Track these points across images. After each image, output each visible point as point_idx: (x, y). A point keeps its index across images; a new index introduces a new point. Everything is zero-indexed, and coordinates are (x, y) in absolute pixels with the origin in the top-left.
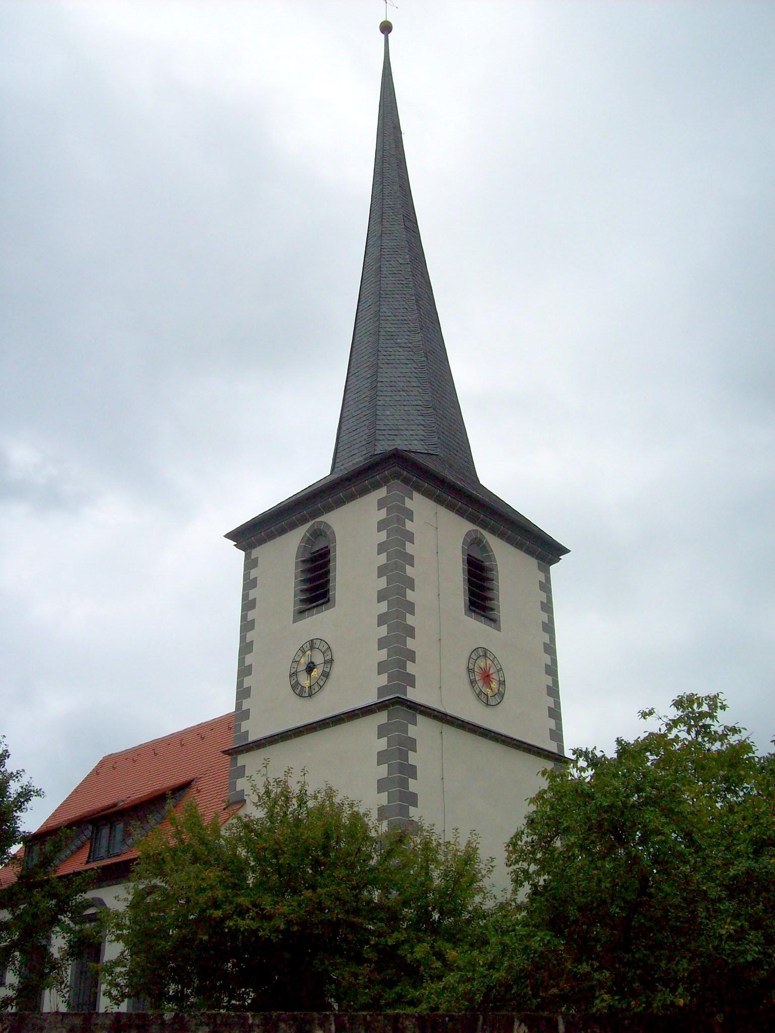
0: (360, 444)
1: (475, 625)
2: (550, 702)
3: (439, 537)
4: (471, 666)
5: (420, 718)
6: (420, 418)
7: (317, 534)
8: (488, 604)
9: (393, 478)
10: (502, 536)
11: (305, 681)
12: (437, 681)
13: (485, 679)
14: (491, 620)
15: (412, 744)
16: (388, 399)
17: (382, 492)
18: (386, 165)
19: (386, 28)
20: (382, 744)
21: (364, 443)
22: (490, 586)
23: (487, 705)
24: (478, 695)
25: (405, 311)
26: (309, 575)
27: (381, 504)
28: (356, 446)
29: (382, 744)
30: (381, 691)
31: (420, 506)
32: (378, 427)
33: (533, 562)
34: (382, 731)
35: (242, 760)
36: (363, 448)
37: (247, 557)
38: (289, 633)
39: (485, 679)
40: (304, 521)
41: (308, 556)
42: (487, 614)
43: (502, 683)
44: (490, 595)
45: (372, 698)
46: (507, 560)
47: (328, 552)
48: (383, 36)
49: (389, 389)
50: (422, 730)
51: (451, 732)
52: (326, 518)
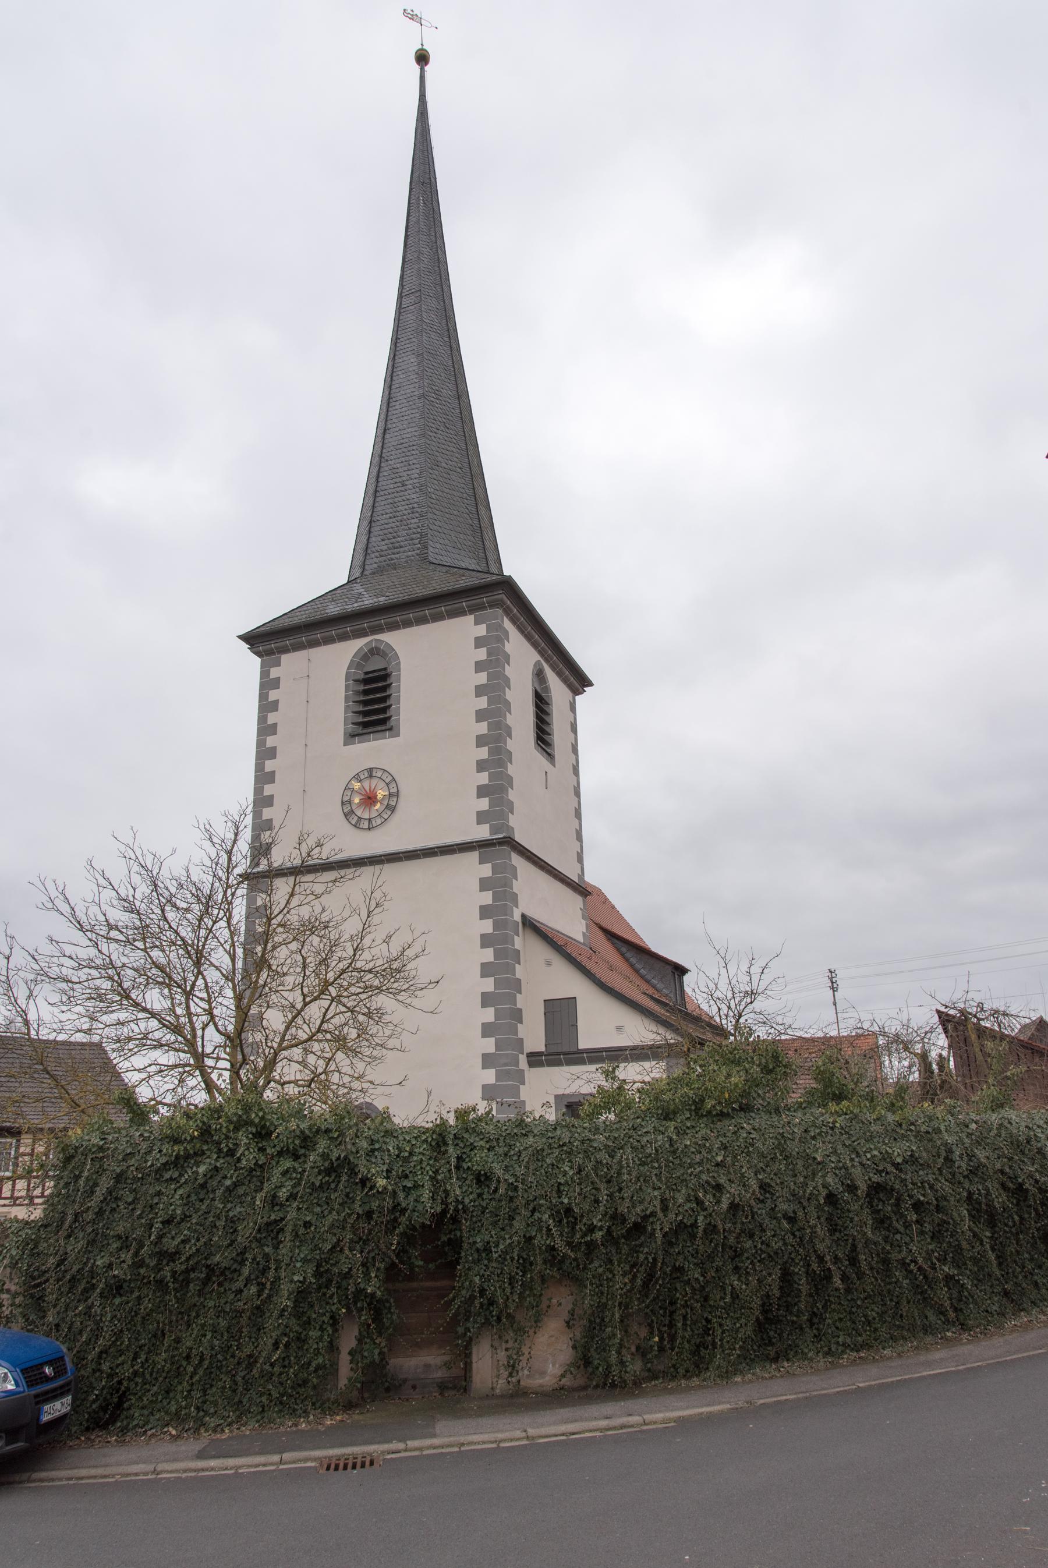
14: (549, 754)
19: (422, 58)
26: (361, 719)
48: (417, 68)
52: (391, 638)
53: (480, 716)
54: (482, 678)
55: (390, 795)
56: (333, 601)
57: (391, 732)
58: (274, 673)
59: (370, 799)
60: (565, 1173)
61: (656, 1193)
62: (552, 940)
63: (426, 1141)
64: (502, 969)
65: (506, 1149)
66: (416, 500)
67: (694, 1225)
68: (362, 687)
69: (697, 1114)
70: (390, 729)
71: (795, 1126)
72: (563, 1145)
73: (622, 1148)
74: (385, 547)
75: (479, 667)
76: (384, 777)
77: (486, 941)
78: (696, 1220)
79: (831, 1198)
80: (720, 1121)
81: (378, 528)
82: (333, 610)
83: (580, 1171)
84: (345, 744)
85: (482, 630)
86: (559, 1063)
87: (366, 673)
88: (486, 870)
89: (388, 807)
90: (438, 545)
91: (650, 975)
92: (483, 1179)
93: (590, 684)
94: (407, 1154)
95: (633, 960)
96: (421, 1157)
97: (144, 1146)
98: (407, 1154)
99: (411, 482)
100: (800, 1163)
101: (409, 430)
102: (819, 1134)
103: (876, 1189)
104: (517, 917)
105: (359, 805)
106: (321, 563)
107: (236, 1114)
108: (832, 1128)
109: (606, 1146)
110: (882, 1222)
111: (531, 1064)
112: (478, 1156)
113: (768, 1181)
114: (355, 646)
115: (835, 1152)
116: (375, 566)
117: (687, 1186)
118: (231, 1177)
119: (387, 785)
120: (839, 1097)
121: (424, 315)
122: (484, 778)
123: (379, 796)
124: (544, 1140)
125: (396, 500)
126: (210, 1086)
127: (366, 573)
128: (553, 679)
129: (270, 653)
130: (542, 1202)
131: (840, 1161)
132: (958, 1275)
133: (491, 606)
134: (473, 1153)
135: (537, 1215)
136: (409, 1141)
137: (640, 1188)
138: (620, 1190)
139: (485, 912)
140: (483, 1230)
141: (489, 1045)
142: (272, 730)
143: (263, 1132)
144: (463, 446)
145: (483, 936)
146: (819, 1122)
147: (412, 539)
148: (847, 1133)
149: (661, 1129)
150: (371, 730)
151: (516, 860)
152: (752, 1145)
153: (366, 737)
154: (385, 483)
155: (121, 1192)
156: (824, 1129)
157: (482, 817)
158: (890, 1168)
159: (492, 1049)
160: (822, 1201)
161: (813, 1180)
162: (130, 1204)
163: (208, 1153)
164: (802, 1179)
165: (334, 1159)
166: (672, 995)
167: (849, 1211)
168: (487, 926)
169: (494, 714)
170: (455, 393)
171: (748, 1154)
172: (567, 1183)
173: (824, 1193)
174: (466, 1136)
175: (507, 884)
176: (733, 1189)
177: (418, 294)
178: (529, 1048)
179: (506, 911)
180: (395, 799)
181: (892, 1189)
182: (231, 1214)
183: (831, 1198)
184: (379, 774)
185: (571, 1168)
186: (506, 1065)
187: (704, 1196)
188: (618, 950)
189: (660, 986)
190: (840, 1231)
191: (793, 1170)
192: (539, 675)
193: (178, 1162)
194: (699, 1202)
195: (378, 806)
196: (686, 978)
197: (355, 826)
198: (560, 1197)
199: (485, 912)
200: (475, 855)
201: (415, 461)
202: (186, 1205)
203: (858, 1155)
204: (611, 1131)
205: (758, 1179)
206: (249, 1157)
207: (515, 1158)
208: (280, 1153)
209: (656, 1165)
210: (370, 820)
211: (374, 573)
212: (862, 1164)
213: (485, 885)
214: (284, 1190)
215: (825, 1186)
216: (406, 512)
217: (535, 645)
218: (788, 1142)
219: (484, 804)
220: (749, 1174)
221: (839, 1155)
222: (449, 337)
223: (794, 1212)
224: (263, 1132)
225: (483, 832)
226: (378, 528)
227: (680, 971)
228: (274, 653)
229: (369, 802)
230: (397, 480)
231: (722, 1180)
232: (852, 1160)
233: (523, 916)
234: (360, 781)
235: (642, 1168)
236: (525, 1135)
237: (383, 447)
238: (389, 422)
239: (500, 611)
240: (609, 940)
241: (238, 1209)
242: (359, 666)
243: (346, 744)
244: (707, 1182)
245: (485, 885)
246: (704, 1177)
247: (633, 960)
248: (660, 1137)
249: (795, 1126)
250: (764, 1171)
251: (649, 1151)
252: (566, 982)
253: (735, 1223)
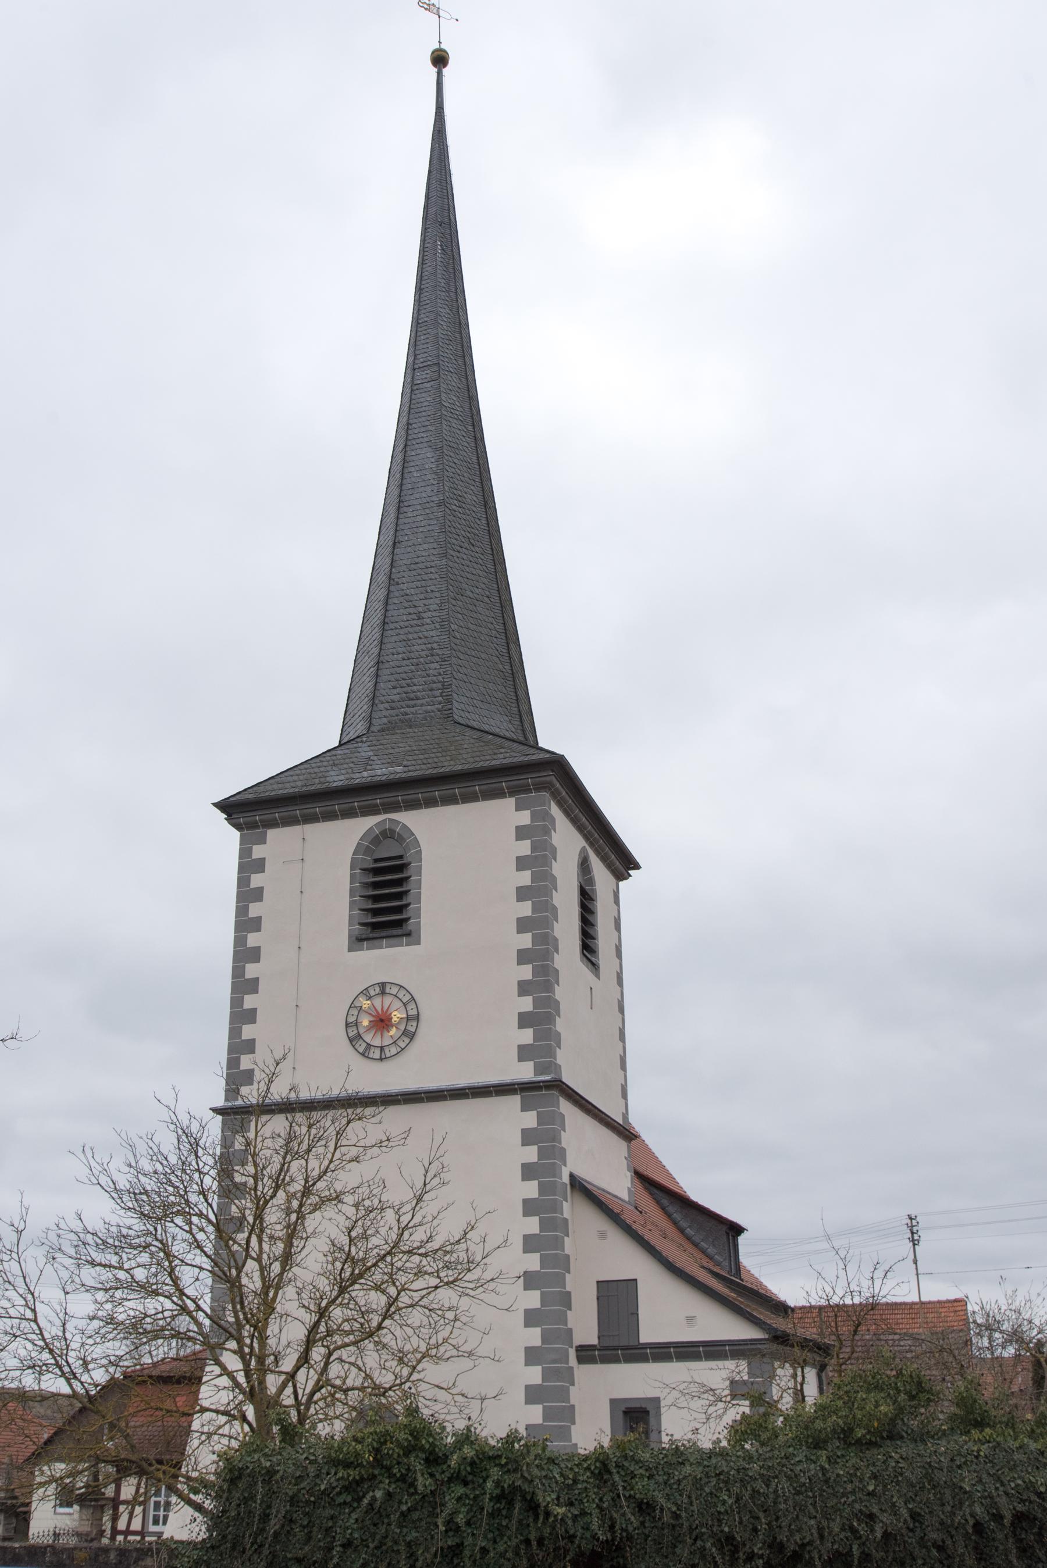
14: (593, 964)
19: (440, 59)
48: (435, 70)
53: (523, 925)
54: (525, 878)
55: (409, 1018)
56: (334, 765)
57: (410, 939)
58: (258, 852)
59: (382, 1022)
60: (724, 1502)
61: (812, 1522)
62: (607, 1207)
63: (588, 1468)
64: (548, 1242)
65: (665, 1478)
66: (436, 639)
67: (849, 1553)
69: (845, 1442)
70: (408, 934)
71: (941, 1455)
72: (720, 1474)
73: (776, 1477)
74: (397, 697)
75: (522, 863)
76: (400, 995)
77: (529, 1207)
78: (851, 1548)
79: (978, 1527)
80: (868, 1449)
81: (388, 672)
82: (337, 779)
83: (737, 1500)
84: (349, 950)
85: (524, 818)
86: (616, 1360)
87: (376, 861)
88: (530, 1120)
89: (405, 1033)
90: (463, 699)
91: (701, 1239)
92: (645, 1507)
93: (637, 867)
94: (571, 1482)
95: (677, 1216)
96: (585, 1485)
97: (312, 1470)
98: (571, 1482)
99: (429, 614)
100: (948, 1493)
101: (426, 546)
102: (965, 1463)
103: (1019, 1517)
104: (566, 1179)
105: (368, 1029)
106: (306, 719)
107: (407, 1439)
108: (977, 1457)
109: (762, 1475)
110: (1024, 1551)
111: (581, 1360)
112: (639, 1485)
113: (918, 1510)
114: (361, 826)
115: (980, 1481)
116: (385, 720)
117: (841, 1516)
118: (406, 1503)
119: (405, 1005)
120: (980, 1424)
121: (444, 396)
122: (526, 1004)
123: (395, 1019)
124: (701, 1468)
125: (410, 636)
127: (373, 729)
128: (597, 865)
129: (253, 826)
130: (704, 1530)
131: (985, 1491)
133: (537, 790)
134: (634, 1481)
135: (699, 1543)
136: (571, 1469)
137: (797, 1516)
138: (777, 1519)
139: (528, 1172)
140: (647, 1558)
141: (534, 1337)
142: (255, 925)
143: (431, 1458)
144: (491, 568)
145: (525, 1202)
146: (964, 1451)
147: (431, 690)
148: (991, 1462)
149: (812, 1457)
150: (382, 934)
151: (565, 1107)
152: (901, 1474)
153: (376, 942)
154: (395, 613)
155: (295, 1515)
156: (969, 1458)
157: (524, 1053)
158: (1034, 1498)
159: (537, 1342)
160: (970, 1531)
161: (961, 1509)
162: (304, 1527)
163: (380, 1478)
164: (949, 1509)
165: (506, 1486)
166: (726, 1264)
167: (993, 1539)
168: (531, 1189)
169: (538, 923)
170: (481, 498)
171: (898, 1483)
172: (726, 1511)
173: (971, 1522)
174: (626, 1464)
175: (555, 1138)
176: (885, 1518)
177: (435, 368)
178: (579, 1339)
179: (553, 1171)
180: (415, 1024)
181: (1035, 1519)
182: (408, 1539)
183: (978, 1527)
184: (394, 990)
185: (730, 1497)
186: (554, 1361)
187: (859, 1525)
188: (658, 1202)
189: (711, 1250)
190: (985, 1560)
191: (941, 1499)
192: (584, 866)
193: (353, 1487)
194: (853, 1530)
195: (393, 1031)
196: (742, 1239)
197: (363, 1054)
198: (720, 1526)
199: (528, 1172)
200: (515, 1100)
201: (433, 588)
202: (361, 1529)
203: (1003, 1484)
204: (765, 1460)
205: (908, 1508)
206: (423, 1483)
207: (675, 1486)
208: (450, 1480)
209: (810, 1494)
210: (382, 1048)
211: (383, 730)
212: (1007, 1494)
213: (528, 1137)
214: (461, 1516)
215: (972, 1515)
216: (423, 654)
217: (580, 829)
218: (935, 1471)
219: (527, 1036)
220: (900, 1503)
221: (984, 1484)
222: (473, 425)
223: (943, 1541)
224: (431, 1458)
225: (526, 1072)
226: (388, 672)
227: (736, 1230)
228: (257, 827)
229: (381, 1023)
230: (411, 610)
231: (875, 1510)
232: (997, 1489)
233: (572, 1176)
234: (370, 998)
235: (797, 1498)
236: (683, 1463)
237: (392, 565)
238: (399, 534)
239: (547, 795)
240: (646, 1188)
241: (415, 1534)
242: (367, 851)
243: (350, 949)
244: (861, 1511)
245: (528, 1137)
246: (857, 1506)
247: (677, 1216)
248: (812, 1466)
249: (941, 1455)
250: (913, 1500)
251: (803, 1480)
252: (624, 1260)
253: (887, 1552)
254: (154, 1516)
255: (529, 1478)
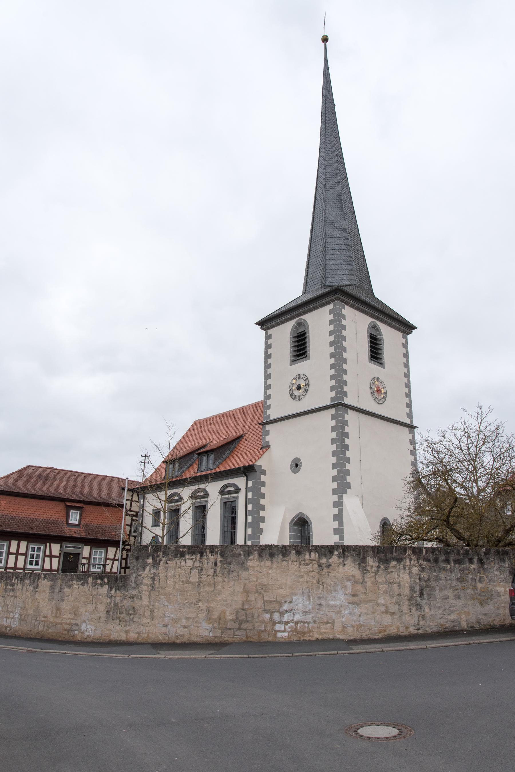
0: (318, 279)
1: (374, 367)
2: (407, 400)
3: (357, 325)
4: (372, 386)
5: (349, 411)
6: (347, 266)
7: (300, 324)
8: (379, 356)
9: (336, 300)
10: (385, 323)
11: (296, 393)
12: (358, 394)
13: (378, 392)
15: (346, 423)
16: (331, 256)
17: (331, 306)
18: (327, 125)
19: (325, 40)
20: (333, 423)
21: (320, 279)
22: (379, 343)
23: (379, 403)
24: (375, 399)
25: (338, 209)
27: (331, 312)
28: (316, 280)
29: (333, 423)
30: (332, 399)
31: (348, 311)
32: (327, 271)
33: (400, 334)
34: (333, 417)
35: (268, 427)
36: (320, 281)
37: (266, 334)
38: (286, 370)
39: (378, 392)
40: (293, 318)
41: (295, 335)
42: (380, 361)
43: (385, 393)
44: (379, 342)
45: (328, 403)
46: (389, 335)
47: (306, 333)
48: (323, 44)
49: (331, 251)
50: (351, 416)
51: (363, 417)
55: (306, 385)
59: (299, 388)
68: (296, 339)
106: (292, 288)
123: (302, 386)
126: (181, 562)
132: (463, 546)
229: (299, 388)
254: (30, 561)
255: (135, 513)
